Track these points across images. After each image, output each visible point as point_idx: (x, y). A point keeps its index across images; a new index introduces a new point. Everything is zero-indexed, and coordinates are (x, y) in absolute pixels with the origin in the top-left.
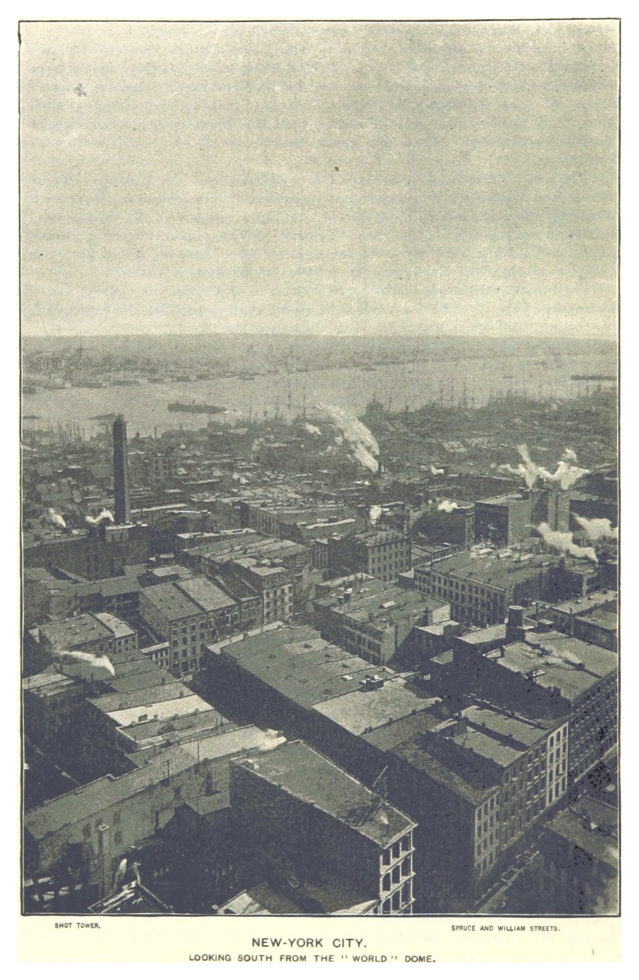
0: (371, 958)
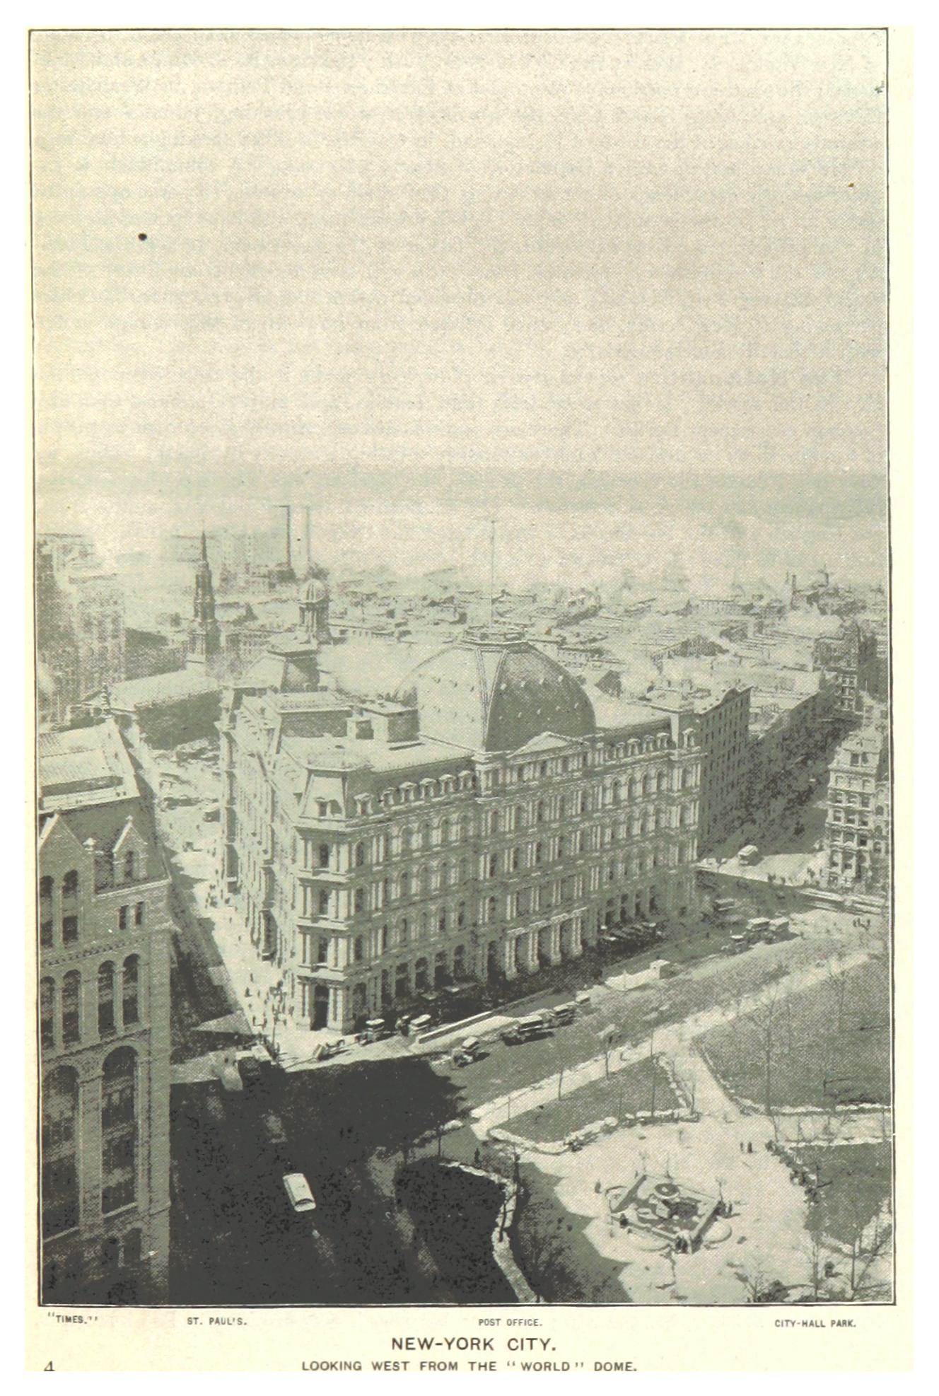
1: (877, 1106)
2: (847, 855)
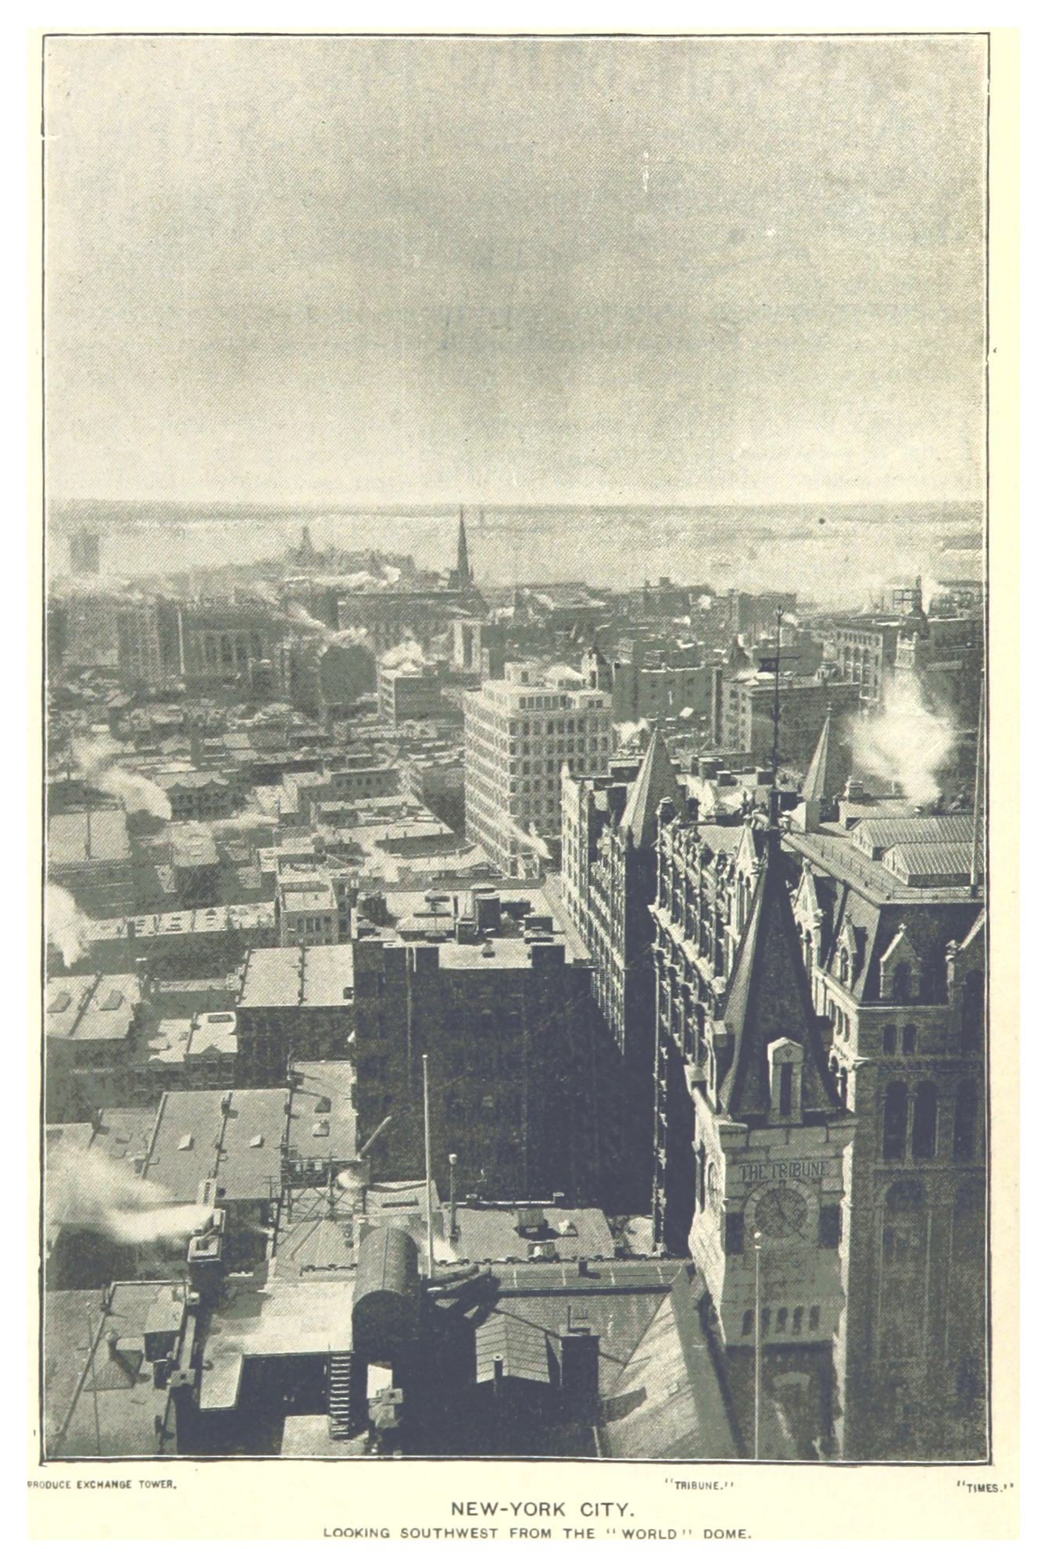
0: (652, 1534)
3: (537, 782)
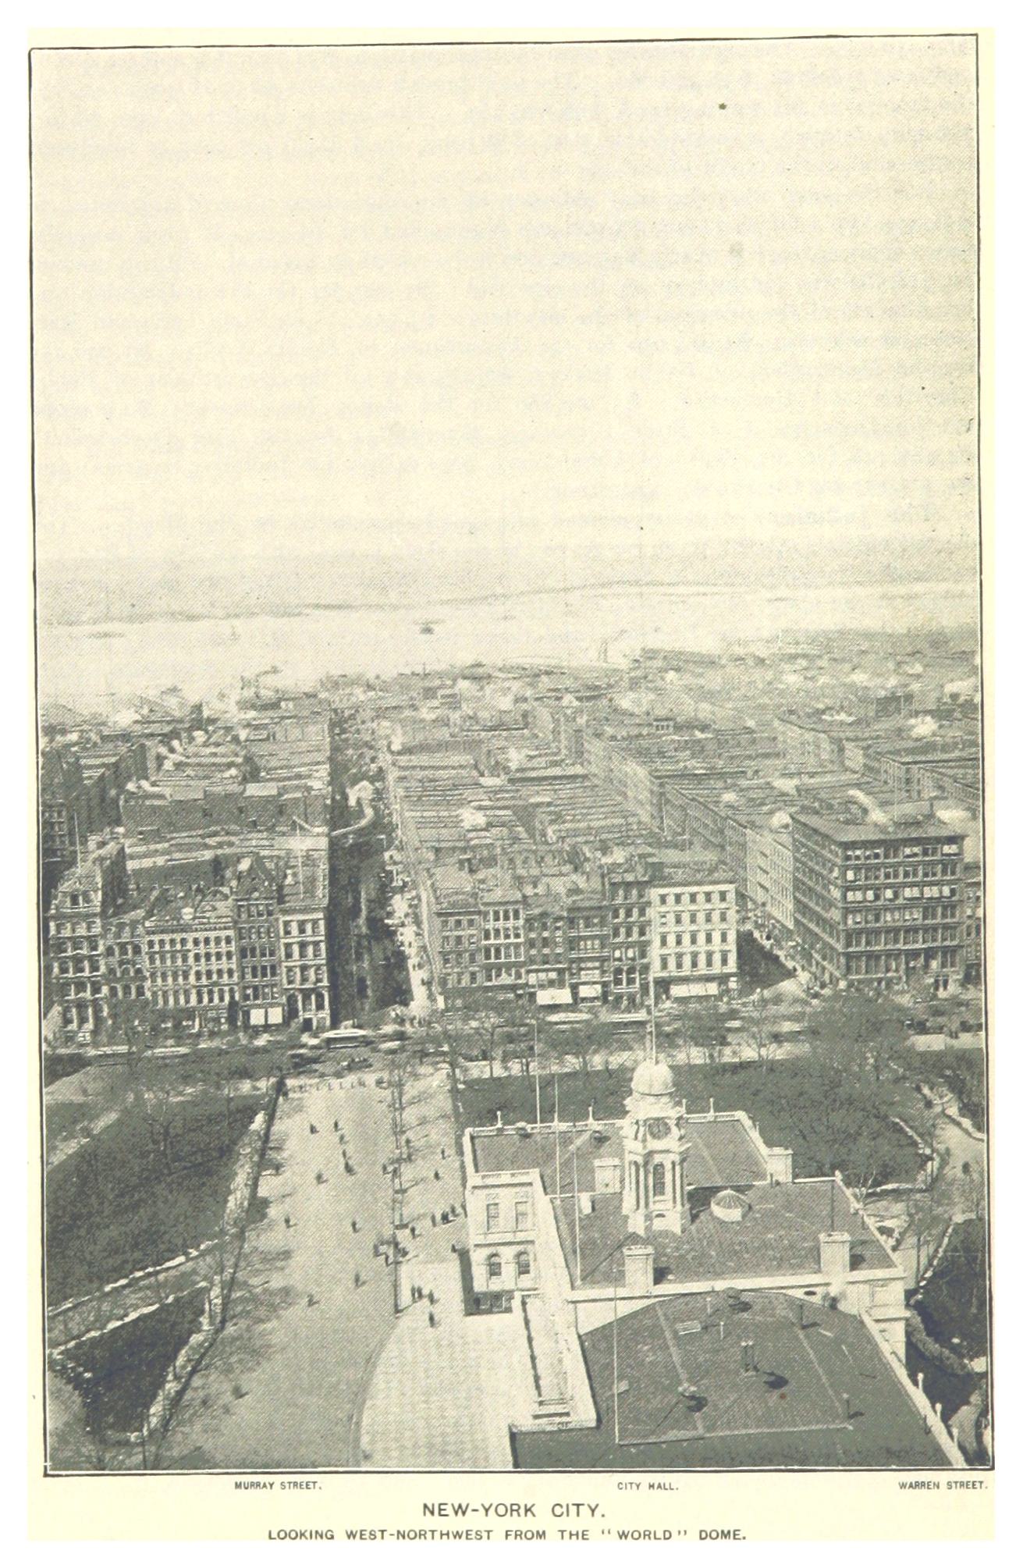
0: (647, 1535)
1: (150, 1270)
2: (81, 1006)
3: (264, 955)
